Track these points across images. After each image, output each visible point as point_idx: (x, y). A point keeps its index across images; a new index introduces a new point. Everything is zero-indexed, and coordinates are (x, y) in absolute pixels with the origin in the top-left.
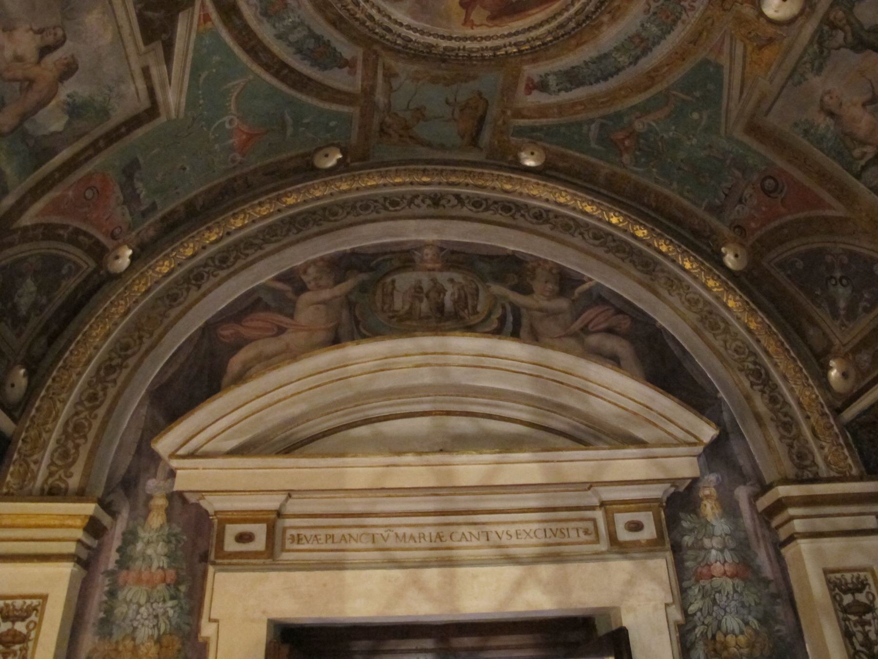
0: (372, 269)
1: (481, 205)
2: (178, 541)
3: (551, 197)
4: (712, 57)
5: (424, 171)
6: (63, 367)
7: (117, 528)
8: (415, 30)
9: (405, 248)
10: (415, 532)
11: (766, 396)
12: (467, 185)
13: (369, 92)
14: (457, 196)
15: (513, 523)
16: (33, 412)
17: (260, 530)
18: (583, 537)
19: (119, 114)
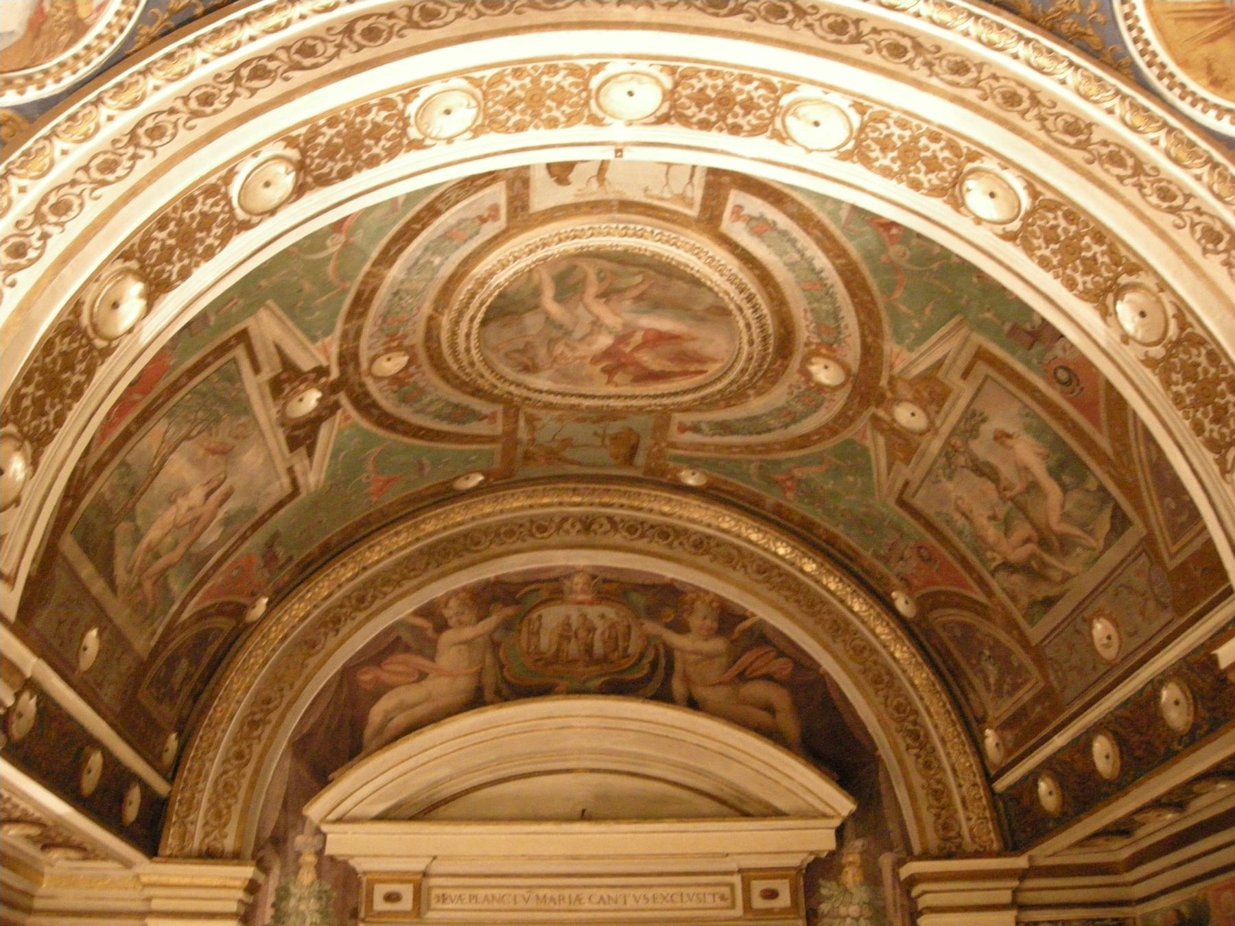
0: (517, 602)
1: (637, 530)
2: (329, 898)
3: (714, 522)
4: (857, 438)
5: (574, 490)
6: (209, 725)
7: (272, 884)
8: (556, 394)
9: (553, 575)
10: (555, 893)
11: (921, 760)
12: (622, 506)
13: (510, 436)
14: (610, 519)
15: (651, 886)
16: (186, 773)
17: (407, 891)
18: (719, 903)
19: (265, 505)
